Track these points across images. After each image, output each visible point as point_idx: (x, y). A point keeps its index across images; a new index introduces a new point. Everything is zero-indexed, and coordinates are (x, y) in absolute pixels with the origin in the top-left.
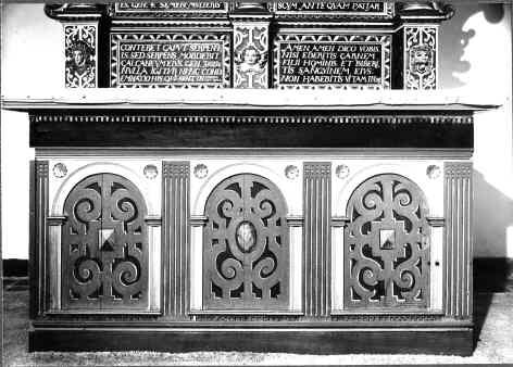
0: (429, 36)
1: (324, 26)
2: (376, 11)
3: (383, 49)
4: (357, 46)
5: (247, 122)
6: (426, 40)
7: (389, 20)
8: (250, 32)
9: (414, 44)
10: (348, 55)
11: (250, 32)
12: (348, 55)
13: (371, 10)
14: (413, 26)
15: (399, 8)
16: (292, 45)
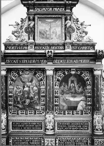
0: (102, 142)
1: (71, 136)
2: (86, 130)
3: (89, 141)
4: (81, 140)
5: (62, 7)
6: (101, 143)
7: (90, 134)
8: (50, 141)
9: (97, 145)
10: (78, 143)
11: (50, 141)
12: (78, 143)
13: (85, 130)
14: (97, 139)
15: (93, 142)
16: (62, 140)
